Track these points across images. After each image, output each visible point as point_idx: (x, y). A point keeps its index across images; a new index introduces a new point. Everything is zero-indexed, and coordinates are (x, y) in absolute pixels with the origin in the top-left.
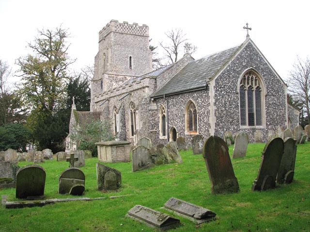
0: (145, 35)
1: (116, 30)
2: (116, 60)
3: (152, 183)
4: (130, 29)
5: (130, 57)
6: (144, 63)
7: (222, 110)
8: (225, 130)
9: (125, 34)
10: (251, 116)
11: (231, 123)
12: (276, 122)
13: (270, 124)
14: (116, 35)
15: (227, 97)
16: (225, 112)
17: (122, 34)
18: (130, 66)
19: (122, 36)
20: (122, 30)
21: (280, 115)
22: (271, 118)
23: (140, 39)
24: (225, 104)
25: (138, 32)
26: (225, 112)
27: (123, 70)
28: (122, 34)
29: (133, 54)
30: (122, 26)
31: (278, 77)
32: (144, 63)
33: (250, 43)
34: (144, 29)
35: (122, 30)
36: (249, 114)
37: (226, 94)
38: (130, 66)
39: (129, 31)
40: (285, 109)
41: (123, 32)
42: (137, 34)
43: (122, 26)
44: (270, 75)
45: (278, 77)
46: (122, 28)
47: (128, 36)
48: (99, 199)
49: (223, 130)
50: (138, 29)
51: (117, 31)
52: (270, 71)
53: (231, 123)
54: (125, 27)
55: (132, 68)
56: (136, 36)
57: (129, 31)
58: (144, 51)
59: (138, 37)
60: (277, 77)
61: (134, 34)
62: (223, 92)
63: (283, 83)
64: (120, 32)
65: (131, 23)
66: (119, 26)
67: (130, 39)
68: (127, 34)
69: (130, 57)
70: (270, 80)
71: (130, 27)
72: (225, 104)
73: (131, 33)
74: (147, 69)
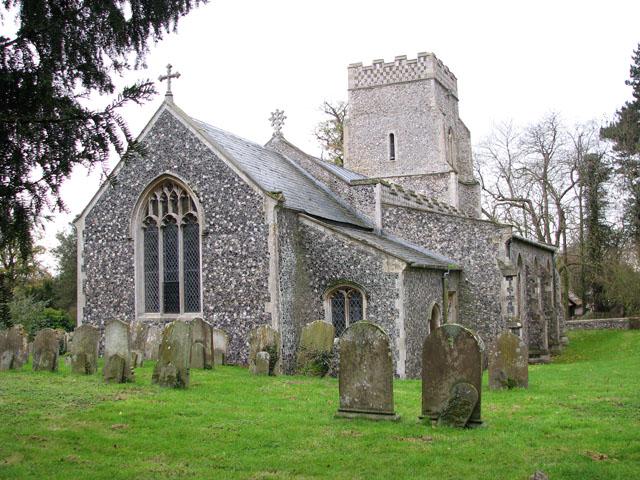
0: (423, 77)
1: (357, 85)
2: (360, 148)
3: (368, 404)
4: (388, 73)
5: (392, 135)
6: (424, 142)
7: (96, 281)
8: (103, 322)
9: (377, 86)
10: (171, 288)
11: (115, 307)
12: (236, 303)
13: (217, 309)
14: (357, 96)
15: (108, 250)
16: (102, 285)
17: (371, 88)
18: (393, 154)
19: (370, 94)
20: (369, 80)
21: (248, 285)
22: (219, 294)
23: (410, 88)
24: (104, 265)
25: (407, 75)
26: (102, 285)
27: (375, 166)
28: (371, 88)
29: (396, 126)
30: (369, 73)
31: (243, 177)
32: (424, 142)
33: (166, 112)
34: (419, 65)
35: (369, 80)
36: (167, 286)
37: (107, 245)
38: (393, 154)
39: (385, 78)
40: (267, 265)
41: (373, 84)
42: (404, 80)
43: (369, 73)
44: (220, 177)
45: (243, 177)
46: (369, 77)
47: (384, 89)
48: (371, 420)
49: (99, 323)
50: (406, 67)
51: (360, 86)
52: (221, 166)
53: (115, 307)
54: (375, 72)
55: (396, 157)
56: (401, 86)
57: (385, 78)
58: (422, 113)
59: (407, 86)
60: (241, 180)
61: (398, 80)
62: (100, 241)
63: (260, 192)
64: (366, 85)
65: (389, 59)
66: (363, 73)
67: (389, 93)
68: (381, 86)
69: (392, 135)
70: (219, 191)
71: (388, 69)
72: (104, 265)
73: (391, 81)
74: (432, 153)
